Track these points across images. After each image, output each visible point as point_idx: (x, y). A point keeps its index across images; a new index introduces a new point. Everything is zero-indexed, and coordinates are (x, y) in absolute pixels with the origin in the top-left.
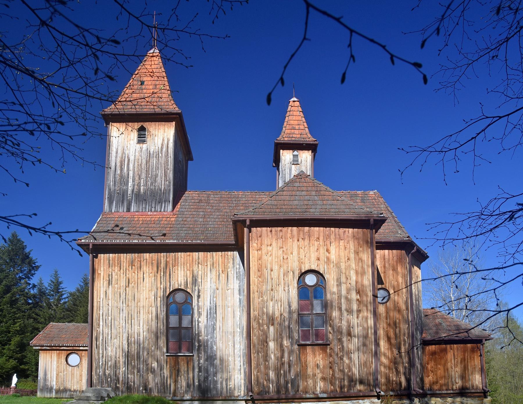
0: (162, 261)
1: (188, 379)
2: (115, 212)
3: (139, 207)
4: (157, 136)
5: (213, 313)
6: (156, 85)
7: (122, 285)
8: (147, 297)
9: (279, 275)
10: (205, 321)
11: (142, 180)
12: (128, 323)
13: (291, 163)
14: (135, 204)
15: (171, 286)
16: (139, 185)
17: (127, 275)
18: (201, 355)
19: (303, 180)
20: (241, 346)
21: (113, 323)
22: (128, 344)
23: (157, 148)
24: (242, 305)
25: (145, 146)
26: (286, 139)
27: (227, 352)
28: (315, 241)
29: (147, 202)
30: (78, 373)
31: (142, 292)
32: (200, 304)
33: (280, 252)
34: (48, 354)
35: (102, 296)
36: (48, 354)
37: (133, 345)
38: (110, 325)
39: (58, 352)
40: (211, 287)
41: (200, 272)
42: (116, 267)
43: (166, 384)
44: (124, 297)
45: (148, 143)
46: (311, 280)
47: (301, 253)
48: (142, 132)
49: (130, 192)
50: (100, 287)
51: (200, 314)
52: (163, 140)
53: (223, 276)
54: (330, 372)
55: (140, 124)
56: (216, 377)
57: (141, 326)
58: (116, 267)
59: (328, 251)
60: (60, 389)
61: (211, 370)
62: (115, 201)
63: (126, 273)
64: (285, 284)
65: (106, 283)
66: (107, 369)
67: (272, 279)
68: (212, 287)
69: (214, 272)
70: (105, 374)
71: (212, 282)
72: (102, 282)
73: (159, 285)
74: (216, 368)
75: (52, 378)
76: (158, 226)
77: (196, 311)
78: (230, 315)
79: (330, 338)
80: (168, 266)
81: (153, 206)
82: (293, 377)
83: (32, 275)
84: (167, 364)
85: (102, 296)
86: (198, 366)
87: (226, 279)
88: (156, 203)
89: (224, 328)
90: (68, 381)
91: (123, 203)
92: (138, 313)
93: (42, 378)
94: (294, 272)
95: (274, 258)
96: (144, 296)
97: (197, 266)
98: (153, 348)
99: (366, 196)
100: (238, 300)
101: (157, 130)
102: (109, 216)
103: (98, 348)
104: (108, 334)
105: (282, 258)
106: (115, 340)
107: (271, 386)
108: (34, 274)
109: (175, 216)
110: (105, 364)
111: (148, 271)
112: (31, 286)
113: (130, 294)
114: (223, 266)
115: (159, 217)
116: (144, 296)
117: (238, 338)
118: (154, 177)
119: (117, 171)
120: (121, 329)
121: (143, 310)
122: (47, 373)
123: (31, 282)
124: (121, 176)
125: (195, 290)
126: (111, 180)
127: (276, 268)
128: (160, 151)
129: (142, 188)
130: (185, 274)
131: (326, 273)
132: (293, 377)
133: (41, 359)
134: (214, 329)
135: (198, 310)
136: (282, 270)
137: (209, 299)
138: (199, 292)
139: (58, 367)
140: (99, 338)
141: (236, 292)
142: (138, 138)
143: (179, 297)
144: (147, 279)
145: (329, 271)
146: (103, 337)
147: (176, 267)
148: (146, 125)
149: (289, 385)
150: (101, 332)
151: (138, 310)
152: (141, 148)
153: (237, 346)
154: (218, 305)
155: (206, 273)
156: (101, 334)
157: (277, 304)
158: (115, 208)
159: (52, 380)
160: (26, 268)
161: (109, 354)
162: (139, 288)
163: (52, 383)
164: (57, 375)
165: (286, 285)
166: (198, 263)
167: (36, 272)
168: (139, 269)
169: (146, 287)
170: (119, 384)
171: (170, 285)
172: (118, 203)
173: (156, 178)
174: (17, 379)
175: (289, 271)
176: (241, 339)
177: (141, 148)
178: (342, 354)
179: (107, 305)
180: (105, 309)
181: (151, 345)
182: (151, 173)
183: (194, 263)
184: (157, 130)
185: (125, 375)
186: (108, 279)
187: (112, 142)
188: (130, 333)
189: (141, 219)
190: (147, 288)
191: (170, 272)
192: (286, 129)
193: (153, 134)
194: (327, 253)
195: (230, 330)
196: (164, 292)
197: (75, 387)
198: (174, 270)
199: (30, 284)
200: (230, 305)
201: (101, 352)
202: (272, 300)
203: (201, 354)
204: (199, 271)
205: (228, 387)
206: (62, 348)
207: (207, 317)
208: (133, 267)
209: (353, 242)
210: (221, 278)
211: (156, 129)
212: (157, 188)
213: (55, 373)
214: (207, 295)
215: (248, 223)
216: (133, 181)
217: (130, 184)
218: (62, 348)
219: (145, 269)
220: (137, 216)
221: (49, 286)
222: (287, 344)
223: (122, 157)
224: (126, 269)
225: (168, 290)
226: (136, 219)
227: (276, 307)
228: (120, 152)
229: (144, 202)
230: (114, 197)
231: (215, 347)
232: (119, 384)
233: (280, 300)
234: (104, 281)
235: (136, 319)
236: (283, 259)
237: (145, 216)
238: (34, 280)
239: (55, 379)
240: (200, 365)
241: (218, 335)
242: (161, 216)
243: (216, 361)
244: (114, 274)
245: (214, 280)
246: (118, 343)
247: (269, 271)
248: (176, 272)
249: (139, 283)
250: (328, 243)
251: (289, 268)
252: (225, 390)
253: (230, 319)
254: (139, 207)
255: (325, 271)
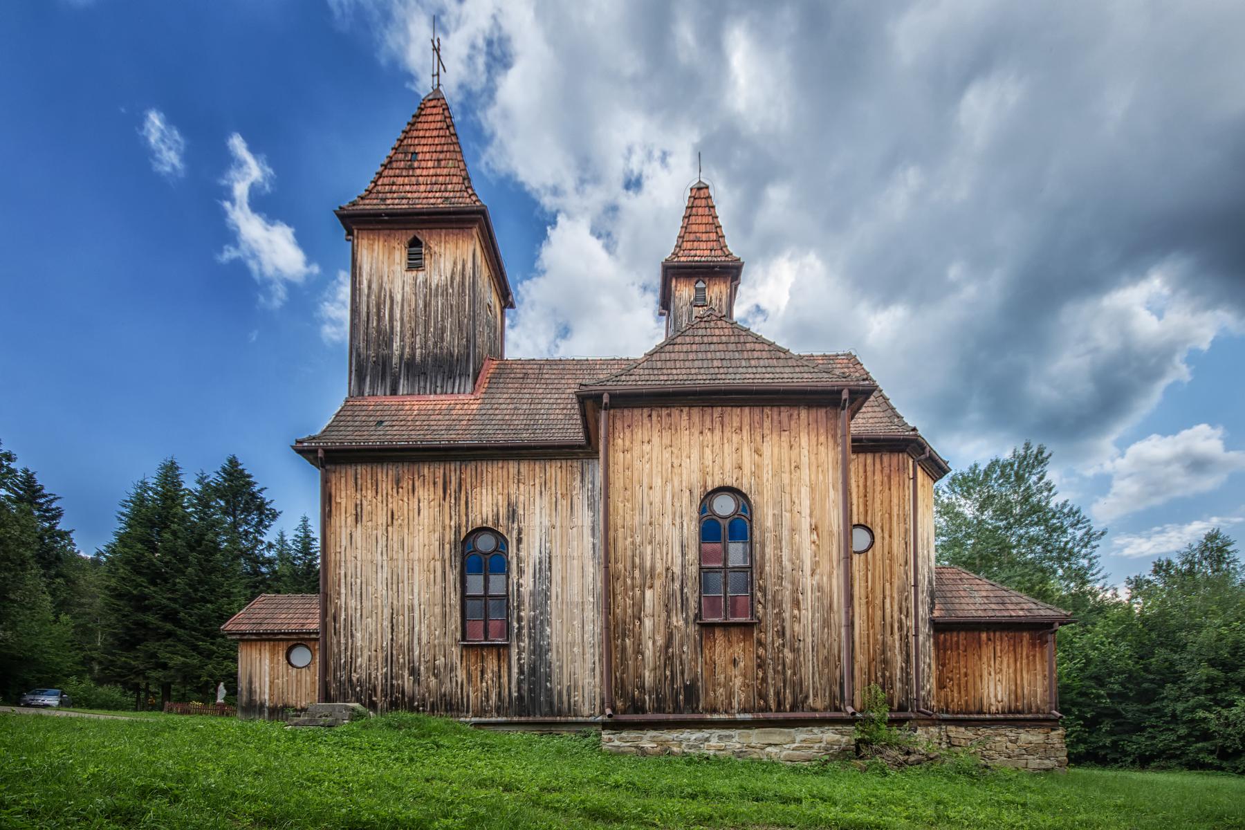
0: (453, 478)
1: (499, 687)
2: (369, 395)
3: (413, 387)
4: (443, 256)
5: (544, 569)
6: (439, 160)
7: (379, 523)
8: (427, 543)
9: (663, 497)
10: (531, 584)
11: (418, 338)
12: (392, 589)
13: (691, 304)
14: (406, 382)
15: (470, 523)
16: (413, 349)
17: (390, 506)
18: (522, 644)
19: (712, 324)
20: (596, 628)
21: (364, 590)
22: (393, 626)
23: (443, 278)
24: (597, 555)
25: (421, 276)
26: (682, 259)
27: (569, 639)
28: (734, 435)
29: (427, 378)
30: (308, 678)
31: (416, 533)
32: (522, 554)
33: (667, 455)
34: (254, 647)
35: (344, 543)
36: (254, 647)
37: (400, 627)
38: (358, 593)
39: (272, 643)
40: (541, 523)
41: (522, 498)
42: (369, 492)
43: (460, 696)
44: (384, 543)
45: (428, 268)
46: (725, 506)
47: (705, 457)
48: (414, 249)
49: (395, 360)
50: (341, 527)
51: (521, 572)
52: (455, 263)
53: (564, 503)
54: (757, 674)
55: (411, 234)
56: (551, 683)
57: (416, 594)
58: (369, 492)
59: (758, 452)
60: (276, 706)
61: (542, 670)
62: (368, 379)
63: (387, 501)
64: (674, 514)
65: (351, 520)
66: (355, 671)
67: (651, 504)
68: (543, 524)
69: (546, 498)
70: (350, 680)
71: (543, 515)
72: (343, 518)
73: (447, 522)
74: (550, 667)
75: (262, 688)
76: (447, 417)
77: (514, 566)
78: (577, 573)
79: (758, 612)
80: (463, 488)
81: (439, 384)
82: (688, 683)
83: (266, 527)
84: (461, 660)
85: (345, 541)
86: (519, 663)
87: (569, 509)
88: (443, 379)
89: (565, 597)
90: (290, 693)
91: (383, 379)
92: (410, 570)
93: (244, 689)
94: (693, 490)
95: (654, 466)
96: (421, 540)
97: (515, 486)
98: (437, 633)
99: (831, 362)
100: (590, 546)
101: (443, 244)
102: (358, 403)
103: (338, 634)
104: (356, 609)
105: (670, 465)
106: (369, 620)
107: (647, 698)
108: (269, 526)
109: (479, 402)
110: (351, 662)
111: (426, 497)
112: (264, 546)
113: (395, 538)
114: (564, 486)
115: (449, 402)
116: (421, 540)
117: (590, 614)
118: (439, 332)
119: (371, 321)
120: (379, 601)
121: (419, 567)
122: (254, 680)
123: (265, 539)
124: (379, 330)
125: (513, 528)
126: (361, 338)
127: (657, 482)
128: (449, 283)
129: (418, 351)
130: (495, 501)
131: (753, 492)
132: (688, 683)
133: (241, 656)
134: (547, 598)
135: (518, 565)
136: (669, 487)
137: (537, 544)
138: (520, 532)
139: (272, 669)
140: (340, 616)
141: (587, 532)
142: (410, 259)
143: (485, 543)
144: (424, 512)
145: (760, 489)
146: (346, 615)
147: (478, 489)
148: (423, 236)
149: (681, 697)
150: (343, 606)
151: (410, 566)
152: (415, 279)
153: (589, 627)
154: (553, 554)
155: (532, 499)
156: (343, 609)
157: (660, 548)
158: (370, 388)
159: (262, 692)
160: (254, 518)
161: (359, 644)
162: (411, 527)
163: (262, 697)
164: (272, 683)
165: (678, 514)
166: (519, 482)
167: (272, 523)
168: (411, 494)
169: (423, 525)
170: (376, 696)
171: (467, 521)
172: (374, 380)
173: (443, 334)
174: (225, 691)
175: (684, 489)
176: (596, 615)
177: (415, 279)
178: (781, 642)
179: (353, 559)
180: (349, 565)
181: (433, 628)
182: (435, 325)
183: (511, 481)
184: (443, 244)
185: (387, 681)
186: (354, 512)
187: (360, 268)
188: (395, 607)
189: (416, 407)
190: (426, 527)
191: (467, 498)
192: (683, 241)
193: (435, 253)
194: (756, 456)
195: (577, 599)
196: (457, 534)
197: (303, 704)
198: (474, 495)
199: (262, 542)
200: (576, 555)
201: (343, 641)
202: (650, 543)
203: (524, 642)
204: (521, 494)
205: (572, 700)
206: (280, 637)
207: (535, 577)
208: (400, 490)
209: (806, 436)
210: (559, 507)
211: (441, 242)
212: (445, 351)
213: (267, 679)
214: (534, 536)
215: (606, 399)
216: (402, 340)
217: (396, 345)
218: (280, 637)
219: (421, 493)
220: (408, 403)
221: (294, 544)
222: (677, 622)
223: (379, 297)
224: (387, 494)
225: (464, 529)
226: (407, 408)
227: (658, 556)
228: (375, 286)
229: (422, 378)
230: (366, 370)
231: (549, 630)
232: (376, 696)
233: (665, 542)
234: (348, 515)
235: (406, 583)
236: (672, 466)
237: (423, 403)
238: (270, 536)
239: (267, 690)
240: (522, 662)
241: (553, 608)
242: (453, 402)
243: (550, 654)
244: (365, 503)
245: (548, 512)
246: (374, 624)
247: (646, 490)
248: (478, 497)
249: (411, 518)
250: (759, 438)
251: (684, 484)
252: (566, 705)
253: (576, 580)
254: (413, 387)
255: (751, 488)
